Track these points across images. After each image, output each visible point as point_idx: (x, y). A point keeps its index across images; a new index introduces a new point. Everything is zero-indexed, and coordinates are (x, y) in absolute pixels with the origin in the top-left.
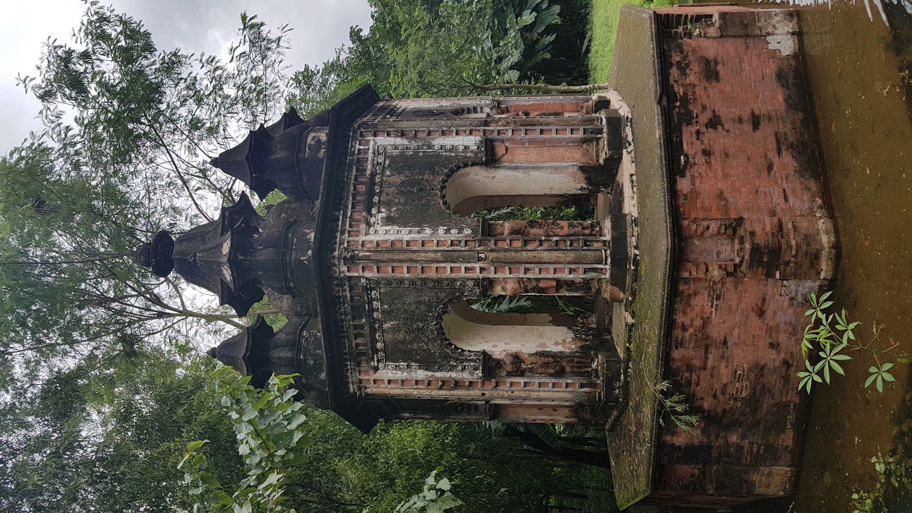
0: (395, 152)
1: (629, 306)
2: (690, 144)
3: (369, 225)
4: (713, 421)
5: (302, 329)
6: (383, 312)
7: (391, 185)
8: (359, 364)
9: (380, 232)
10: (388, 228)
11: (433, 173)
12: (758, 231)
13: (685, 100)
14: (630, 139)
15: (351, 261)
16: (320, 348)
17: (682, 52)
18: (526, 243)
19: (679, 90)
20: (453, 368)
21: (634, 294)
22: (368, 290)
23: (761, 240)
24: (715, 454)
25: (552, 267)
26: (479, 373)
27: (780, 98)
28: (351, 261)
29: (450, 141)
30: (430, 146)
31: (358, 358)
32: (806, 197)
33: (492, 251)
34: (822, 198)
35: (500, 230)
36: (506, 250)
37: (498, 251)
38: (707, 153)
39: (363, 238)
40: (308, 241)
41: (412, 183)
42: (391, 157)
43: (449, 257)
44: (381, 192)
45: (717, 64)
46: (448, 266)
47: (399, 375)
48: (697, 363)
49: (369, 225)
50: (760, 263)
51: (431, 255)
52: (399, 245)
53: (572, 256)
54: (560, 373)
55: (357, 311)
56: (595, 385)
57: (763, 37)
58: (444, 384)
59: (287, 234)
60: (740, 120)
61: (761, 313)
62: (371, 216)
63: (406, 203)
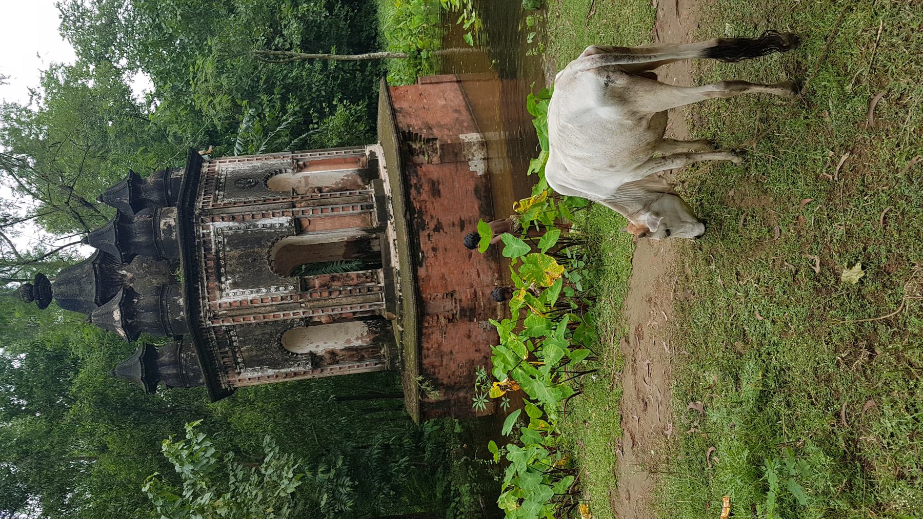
0: (230, 232)
1: (399, 322)
2: (425, 245)
3: (221, 290)
4: (449, 388)
5: (180, 352)
6: (240, 342)
7: (231, 258)
8: (227, 373)
9: (231, 295)
10: (235, 291)
11: (261, 246)
12: (464, 298)
13: (421, 213)
14: (392, 213)
15: (215, 317)
16: (197, 364)
17: (417, 176)
18: (330, 293)
19: (417, 205)
20: (291, 366)
21: (401, 316)
22: (228, 331)
23: (465, 304)
24: (452, 402)
25: (349, 307)
26: (309, 366)
27: (476, 207)
28: (215, 317)
29: (269, 221)
30: (255, 226)
31: (225, 369)
32: (490, 273)
33: (309, 301)
34: (498, 273)
35: (312, 283)
36: (318, 300)
37: (314, 301)
38: (434, 249)
39: (220, 301)
40: (179, 305)
41: (246, 256)
42: (228, 236)
43: (280, 308)
44: (225, 264)
45: (439, 184)
46: (281, 314)
47: (256, 374)
48: (437, 364)
49: (221, 290)
50: (465, 316)
51: (269, 308)
52: (245, 304)
53: (361, 299)
54: (362, 359)
55: (221, 344)
56: (384, 363)
57: (466, 163)
58: (287, 375)
59: (161, 302)
60: (453, 224)
61: (469, 337)
62: (222, 283)
63: (245, 272)
